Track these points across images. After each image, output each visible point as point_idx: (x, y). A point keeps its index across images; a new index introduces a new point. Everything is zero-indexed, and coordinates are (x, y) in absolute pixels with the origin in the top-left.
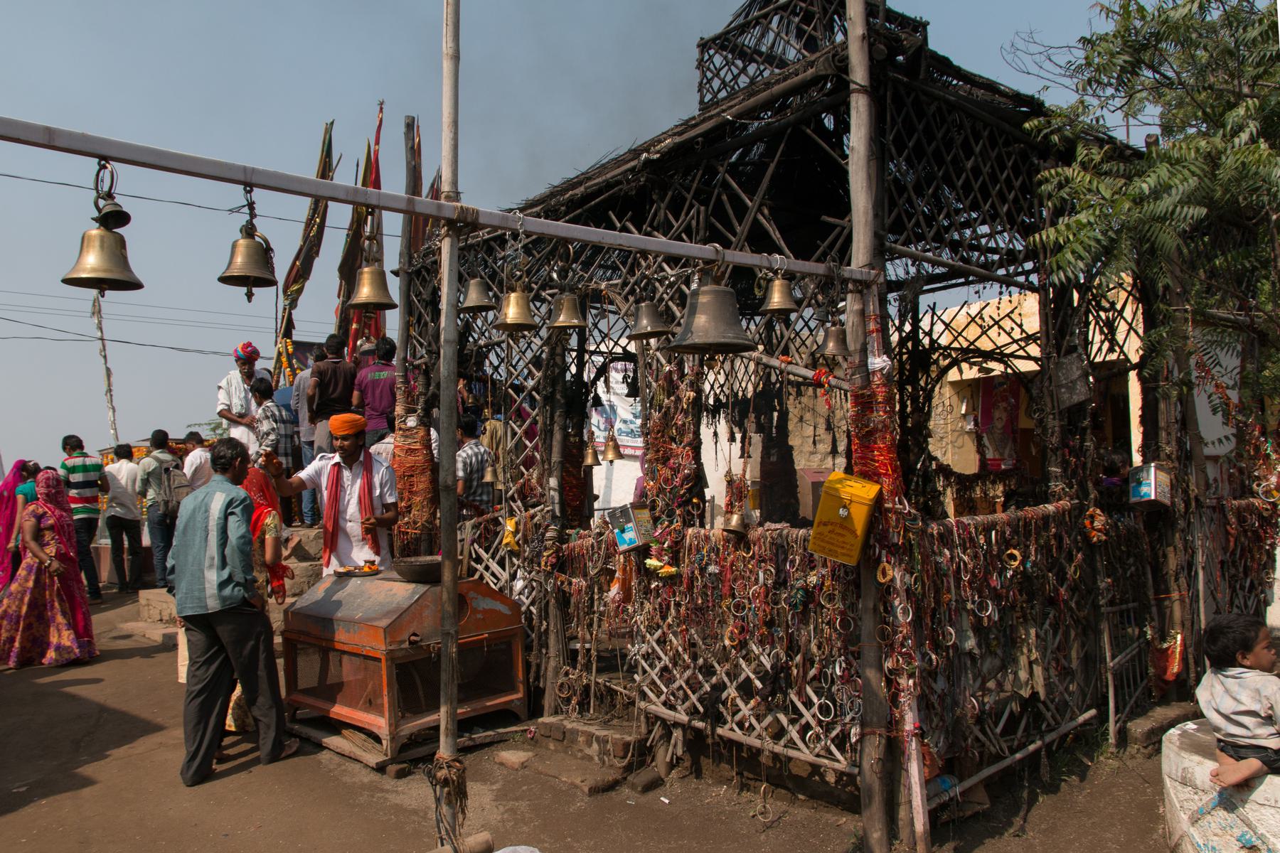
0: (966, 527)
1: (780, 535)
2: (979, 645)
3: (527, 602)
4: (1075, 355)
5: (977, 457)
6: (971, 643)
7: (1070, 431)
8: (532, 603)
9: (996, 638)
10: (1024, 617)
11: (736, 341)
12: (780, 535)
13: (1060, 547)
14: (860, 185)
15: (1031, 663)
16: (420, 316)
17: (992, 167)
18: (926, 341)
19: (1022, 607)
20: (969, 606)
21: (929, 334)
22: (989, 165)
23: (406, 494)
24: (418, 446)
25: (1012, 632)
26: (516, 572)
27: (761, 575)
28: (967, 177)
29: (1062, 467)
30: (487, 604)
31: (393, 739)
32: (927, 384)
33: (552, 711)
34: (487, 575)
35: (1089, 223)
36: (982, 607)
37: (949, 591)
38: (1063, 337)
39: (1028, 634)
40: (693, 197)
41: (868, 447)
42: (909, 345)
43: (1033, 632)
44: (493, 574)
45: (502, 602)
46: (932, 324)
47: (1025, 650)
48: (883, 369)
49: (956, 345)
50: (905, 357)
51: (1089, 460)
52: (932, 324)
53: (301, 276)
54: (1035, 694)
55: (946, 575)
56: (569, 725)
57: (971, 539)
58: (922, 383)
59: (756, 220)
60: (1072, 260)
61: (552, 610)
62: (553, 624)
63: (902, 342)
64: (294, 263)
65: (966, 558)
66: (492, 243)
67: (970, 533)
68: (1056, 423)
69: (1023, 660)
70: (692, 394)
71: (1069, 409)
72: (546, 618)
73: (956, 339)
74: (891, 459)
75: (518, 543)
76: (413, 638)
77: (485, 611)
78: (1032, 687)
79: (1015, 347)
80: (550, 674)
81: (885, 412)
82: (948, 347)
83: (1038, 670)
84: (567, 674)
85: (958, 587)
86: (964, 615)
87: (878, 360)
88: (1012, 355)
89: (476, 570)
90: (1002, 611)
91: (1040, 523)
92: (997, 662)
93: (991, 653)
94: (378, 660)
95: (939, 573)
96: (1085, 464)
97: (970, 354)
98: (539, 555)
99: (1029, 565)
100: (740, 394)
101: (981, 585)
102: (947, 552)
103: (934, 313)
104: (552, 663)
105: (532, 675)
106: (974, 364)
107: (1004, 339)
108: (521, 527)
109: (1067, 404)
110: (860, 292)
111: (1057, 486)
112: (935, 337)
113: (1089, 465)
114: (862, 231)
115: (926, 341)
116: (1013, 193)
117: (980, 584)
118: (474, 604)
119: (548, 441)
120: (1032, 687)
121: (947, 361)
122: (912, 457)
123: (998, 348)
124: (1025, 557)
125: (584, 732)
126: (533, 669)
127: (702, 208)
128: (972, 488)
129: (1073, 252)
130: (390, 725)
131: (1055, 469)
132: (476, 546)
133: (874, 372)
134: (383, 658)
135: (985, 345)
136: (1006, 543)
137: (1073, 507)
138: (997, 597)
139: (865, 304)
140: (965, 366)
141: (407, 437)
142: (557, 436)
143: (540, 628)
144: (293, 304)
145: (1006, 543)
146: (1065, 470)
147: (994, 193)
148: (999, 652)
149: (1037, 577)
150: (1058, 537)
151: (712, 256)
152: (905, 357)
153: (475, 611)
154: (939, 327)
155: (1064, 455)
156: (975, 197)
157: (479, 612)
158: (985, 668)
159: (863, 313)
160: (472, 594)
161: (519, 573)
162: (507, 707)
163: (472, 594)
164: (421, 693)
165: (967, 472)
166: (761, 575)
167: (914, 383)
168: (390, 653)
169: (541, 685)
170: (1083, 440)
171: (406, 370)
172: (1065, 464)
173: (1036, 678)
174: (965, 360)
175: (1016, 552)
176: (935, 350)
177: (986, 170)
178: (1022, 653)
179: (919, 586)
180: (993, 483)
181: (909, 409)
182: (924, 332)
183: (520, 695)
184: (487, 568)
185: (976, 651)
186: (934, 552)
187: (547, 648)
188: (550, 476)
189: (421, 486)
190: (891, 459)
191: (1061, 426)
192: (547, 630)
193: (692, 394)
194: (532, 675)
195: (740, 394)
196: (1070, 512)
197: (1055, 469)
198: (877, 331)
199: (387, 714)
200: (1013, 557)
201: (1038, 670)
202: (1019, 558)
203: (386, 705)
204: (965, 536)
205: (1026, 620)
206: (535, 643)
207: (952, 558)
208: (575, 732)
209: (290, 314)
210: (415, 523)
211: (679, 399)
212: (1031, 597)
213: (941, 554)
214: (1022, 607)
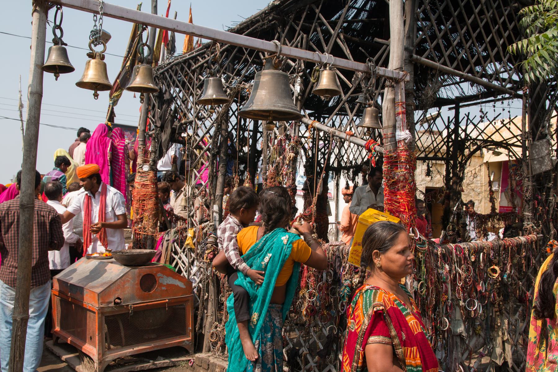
0: (462, 250)
1: (338, 249)
2: (467, 330)
3: (198, 280)
4: (545, 140)
5: (491, 204)
6: (461, 329)
7: (539, 189)
8: (200, 282)
9: (481, 324)
10: (500, 311)
11: (283, 109)
12: (338, 249)
13: (528, 266)
14: (396, 14)
15: (504, 342)
16: (154, 106)
17: (493, 13)
18: (463, 135)
19: (499, 305)
20: (461, 303)
21: (465, 131)
22: (491, 12)
23: (140, 211)
24: (148, 183)
25: (492, 321)
26: (193, 262)
27: (324, 275)
28: (475, 17)
29: (532, 213)
30: (171, 281)
31: (100, 363)
32: (462, 160)
33: (207, 349)
34: (180, 262)
35: (554, 36)
36: (471, 304)
37: (446, 292)
38: (537, 129)
39: (502, 323)
40: (300, 30)
41: (393, 193)
42: (453, 137)
43: (506, 321)
44: (183, 262)
45: (180, 280)
46: (467, 125)
47: (500, 333)
48: (405, 139)
49: (480, 138)
50: (450, 144)
51: (551, 209)
52: (467, 125)
53: (120, 88)
54: (505, 363)
55: (445, 282)
56: (212, 360)
57: (465, 258)
58: (460, 159)
59: (336, 42)
60: (540, 62)
61: (211, 287)
62: (211, 295)
63: (449, 136)
64: (116, 81)
65: (460, 271)
66: (191, 61)
67: (464, 254)
68: (530, 183)
69: (499, 340)
70: (292, 155)
71: (539, 175)
72: (208, 292)
73: (480, 134)
74: (408, 201)
75: (194, 244)
76: (117, 301)
77: (168, 285)
78: (504, 358)
79: (515, 140)
80: (207, 326)
81: (406, 169)
82: (476, 139)
83: (508, 347)
84: (216, 327)
85: (453, 290)
86: (458, 309)
87: (403, 133)
88: (513, 145)
89: (174, 259)
90: (485, 307)
91: (515, 249)
92: (481, 340)
93: (476, 334)
94: (94, 313)
95: (440, 280)
96: (548, 211)
97: (489, 143)
98: (203, 252)
99: (505, 277)
100: (354, 162)
101: (471, 289)
102: (447, 267)
103: (468, 119)
104: (209, 320)
105: (198, 326)
106: (490, 149)
107: (509, 135)
108: (197, 234)
109: (538, 172)
110: (392, 87)
111: (528, 225)
112: (468, 132)
113: (551, 212)
114: (396, 45)
115: (463, 135)
116: (507, 32)
117: (470, 291)
118: (160, 281)
119: (214, 183)
120: (504, 358)
121: (475, 147)
122: (451, 203)
123: (505, 140)
124: (503, 271)
125: (219, 366)
126: (199, 321)
127: (305, 36)
128: (486, 223)
129: (541, 57)
130: (99, 354)
131: (528, 214)
132: (175, 244)
133: (400, 141)
134: (96, 311)
135: (497, 138)
136: (489, 262)
137: (539, 240)
138: (482, 297)
139: (395, 94)
140: (484, 150)
141: (142, 177)
142: (220, 179)
143: (203, 297)
144: (115, 103)
145: (489, 262)
146: (535, 215)
147: (494, 31)
148: (482, 334)
149: (511, 285)
150: (528, 259)
151: (273, 49)
152: (450, 144)
153: (161, 285)
154: (471, 127)
155: (534, 204)
156: (480, 32)
157: (164, 286)
158: (472, 345)
159: (394, 101)
160: (159, 275)
161: (195, 263)
162: (179, 345)
163: (159, 275)
164: (123, 334)
165: (486, 213)
166: (324, 275)
167: (455, 159)
168: (101, 309)
169: (203, 332)
170: (548, 196)
171: (145, 137)
172: (534, 211)
173: (506, 352)
174: (485, 147)
175: (497, 268)
176: (469, 140)
177: (489, 15)
178: (499, 336)
179: (424, 290)
180: (499, 220)
181: (451, 175)
182: (462, 130)
183: (190, 338)
184: (180, 258)
185: (464, 334)
186: (437, 266)
187: (207, 310)
188: (214, 203)
189: (149, 206)
190: (408, 201)
191: (533, 186)
192: (208, 298)
193: (292, 155)
194: (198, 326)
195: (354, 162)
196: (536, 242)
197: (528, 214)
198: (403, 113)
199: (97, 347)
200: (494, 271)
201: (508, 347)
202: (499, 271)
203: (97, 342)
204: (462, 256)
205: (501, 314)
206: (200, 306)
207: (450, 271)
208: (215, 365)
209: (113, 109)
210: (144, 228)
211: (284, 158)
212: (506, 299)
213: (442, 268)
214: (499, 305)
